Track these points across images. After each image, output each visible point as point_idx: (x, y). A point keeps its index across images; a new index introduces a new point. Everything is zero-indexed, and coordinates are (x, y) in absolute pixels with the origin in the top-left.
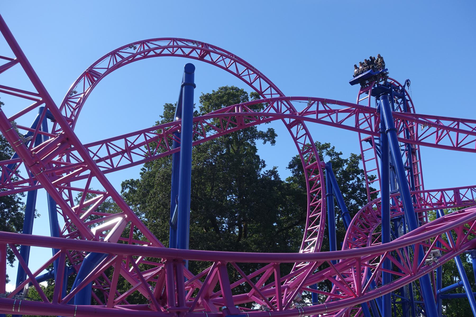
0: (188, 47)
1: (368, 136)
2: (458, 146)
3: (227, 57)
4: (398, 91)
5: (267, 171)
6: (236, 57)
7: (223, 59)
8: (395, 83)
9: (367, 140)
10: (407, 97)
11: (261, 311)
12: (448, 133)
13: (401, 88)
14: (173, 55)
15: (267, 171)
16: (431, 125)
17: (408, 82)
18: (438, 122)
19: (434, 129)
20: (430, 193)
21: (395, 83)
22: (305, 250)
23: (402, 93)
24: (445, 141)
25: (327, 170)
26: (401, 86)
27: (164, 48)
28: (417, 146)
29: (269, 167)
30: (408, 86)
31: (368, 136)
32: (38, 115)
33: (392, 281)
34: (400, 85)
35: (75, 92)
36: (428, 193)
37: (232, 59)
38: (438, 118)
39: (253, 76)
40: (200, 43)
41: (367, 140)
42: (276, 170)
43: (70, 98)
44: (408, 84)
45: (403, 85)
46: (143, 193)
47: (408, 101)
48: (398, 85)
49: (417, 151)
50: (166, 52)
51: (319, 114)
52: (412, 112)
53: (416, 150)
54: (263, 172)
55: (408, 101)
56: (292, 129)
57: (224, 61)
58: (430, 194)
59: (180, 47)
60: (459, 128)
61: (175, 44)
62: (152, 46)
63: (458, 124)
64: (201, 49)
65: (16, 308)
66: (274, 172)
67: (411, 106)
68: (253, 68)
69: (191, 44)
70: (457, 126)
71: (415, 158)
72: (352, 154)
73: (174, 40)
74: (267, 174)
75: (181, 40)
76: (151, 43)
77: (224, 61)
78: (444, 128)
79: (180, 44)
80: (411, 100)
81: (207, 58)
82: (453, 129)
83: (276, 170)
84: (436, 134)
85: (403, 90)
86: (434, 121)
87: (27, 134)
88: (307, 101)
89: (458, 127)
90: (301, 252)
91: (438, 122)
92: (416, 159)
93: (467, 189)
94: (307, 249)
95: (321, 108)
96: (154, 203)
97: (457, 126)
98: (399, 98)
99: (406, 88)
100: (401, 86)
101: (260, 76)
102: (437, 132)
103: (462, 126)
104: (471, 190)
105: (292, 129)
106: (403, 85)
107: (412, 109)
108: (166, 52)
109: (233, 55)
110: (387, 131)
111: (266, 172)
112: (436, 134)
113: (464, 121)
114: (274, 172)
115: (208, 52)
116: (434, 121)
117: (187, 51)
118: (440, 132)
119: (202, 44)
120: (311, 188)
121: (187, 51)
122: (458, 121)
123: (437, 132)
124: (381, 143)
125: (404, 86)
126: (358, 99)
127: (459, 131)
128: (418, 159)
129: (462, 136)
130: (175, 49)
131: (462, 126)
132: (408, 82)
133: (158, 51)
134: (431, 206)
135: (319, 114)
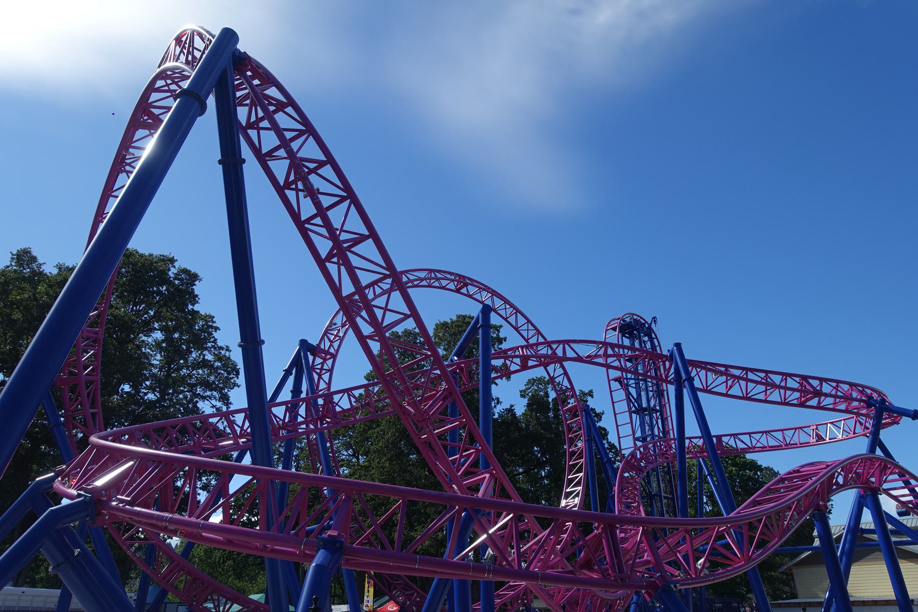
0: (446, 279)
1: (618, 374)
2: (748, 396)
3: (483, 290)
4: (645, 328)
5: (503, 409)
6: (492, 290)
7: (480, 292)
8: (641, 320)
9: (616, 380)
10: (653, 336)
11: (679, 577)
12: (738, 381)
13: (647, 326)
14: (430, 286)
15: (503, 409)
16: (721, 373)
17: (654, 319)
18: (726, 370)
19: (723, 378)
20: (692, 440)
21: (641, 320)
22: (567, 501)
23: (649, 332)
24: (735, 391)
25: (585, 412)
26: (648, 324)
27: (422, 280)
28: (664, 384)
29: (505, 405)
30: (655, 324)
31: (618, 374)
32: (298, 347)
33: (72, 489)
34: (646, 322)
35: (335, 324)
36: (690, 440)
37: (488, 292)
38: (726, 366)
39: (510, 310)
40: (457, 274)
41: (616, 380)
42: (513, 408)
43: (331, 330)
44: (655, 321)
45: (649, 322)
46: (363, 428)
47: (654, 338)
48: (643, 322)
49: (665, 392)
50: (424, 283)
51: (412, 318)
52: (659, 351)
53: (664, 391)
54: (498, 410)
55: (654, 338)
56: (548, 368)
57: (338, 402)
58: (691, 441)
59: (438, 279)
60: (237, 93)
61: (433, 275)
62: (412, 278)
63: (746, 374)
64: (458, 281)
65: (489, 574)
66: (510, 410)
67: (657, 344)
68: (509, 302)
69: (449, 276)
70: (745, 375)
71: (663, 400)
72: (581, 391)
73: (431, 271)
74: (503, 412)
75: (439, 271)
76: (410, 274)
77: (338, 402)
78: (733, 376)
79: (438, 275)
80: (657, 338)
81: (464, 290)
82: (742, 379)
83: (513, 408)
84: (725, 383)
85: (650, 328)
86: (723, 369)
87: (288, 368)
88: (595, 345)
89: (747, 376)
90: (563, 503)
91: (726, 370)
92: (665, 402)
93: (730, 437)
94: (571, 499)
95: (610, 351)
96: (382, 442)
97: (745, 375)
98: (645, 335)
99: (653, 325)
100: (648, 324)
101: (518, 311)
102: (726, 381)
103: (751, 376)
104: (734, 438)
105: (548, 368)
106: (649, 322)
107: (658, 348)
108: (424, 283)
109: (489, 288)
110: (684, 381)
111: (502, 411)
112: (725, 383)
113: (752, 370)
114: (510, 410)
115: (466, 285)
116: (723, 369)
117: (444, 283)
118: (730, 383)
119: (460, 276)
120: (569, 433)
121: (444, 283)
122: (747, 370)
123: (726, 381)
124: (665, 388)
125: (651, 323)
126: (605, 336)
127: (747, 380)
128: (667, 401)
129: (751, 385)
130: (432, 281)
131: (751, 376)
132: (654, 319)
133: (416, 283)
134: (694, 454)
135: (412, 318)
